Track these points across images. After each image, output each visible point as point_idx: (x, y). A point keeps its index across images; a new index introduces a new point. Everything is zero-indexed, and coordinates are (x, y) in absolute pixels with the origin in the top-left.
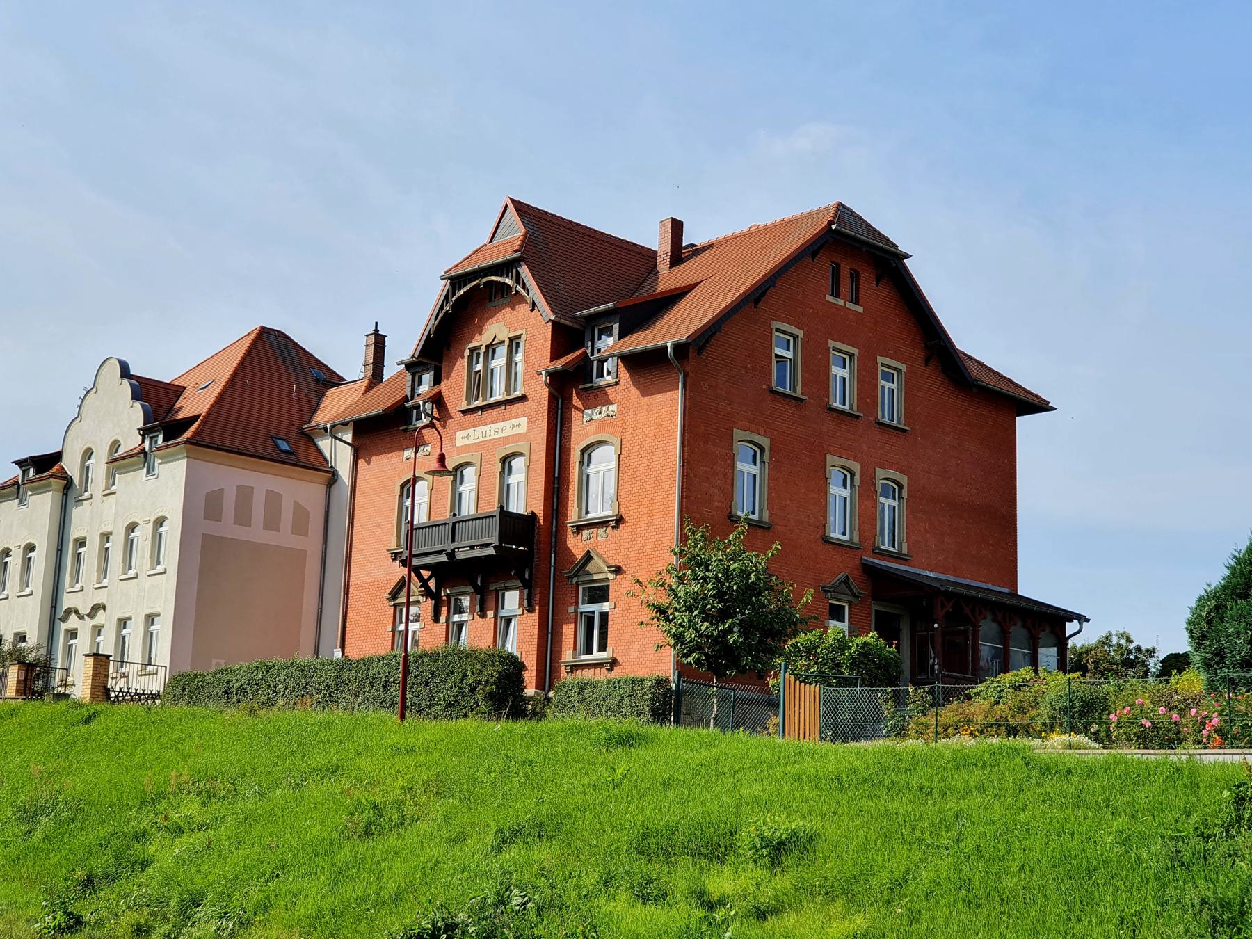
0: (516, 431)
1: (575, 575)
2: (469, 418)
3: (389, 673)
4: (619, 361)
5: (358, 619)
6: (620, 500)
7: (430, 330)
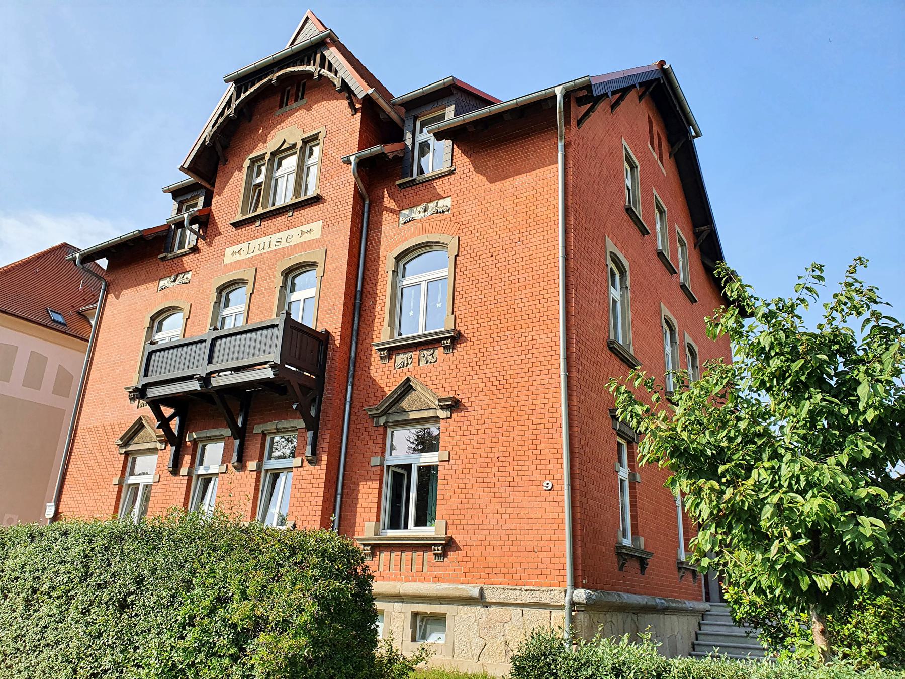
0: (307, 238)
1: (384, 413)
2: (244, 231)
3: (44, 569)
4: (455, 147)
5: (80, 469)
6: (456, 313)
7: (205, 139)
